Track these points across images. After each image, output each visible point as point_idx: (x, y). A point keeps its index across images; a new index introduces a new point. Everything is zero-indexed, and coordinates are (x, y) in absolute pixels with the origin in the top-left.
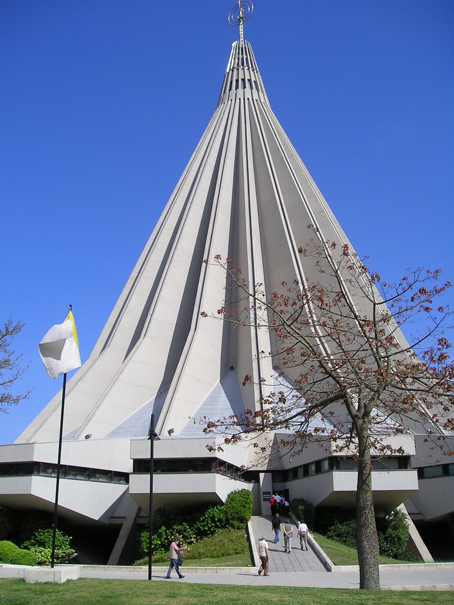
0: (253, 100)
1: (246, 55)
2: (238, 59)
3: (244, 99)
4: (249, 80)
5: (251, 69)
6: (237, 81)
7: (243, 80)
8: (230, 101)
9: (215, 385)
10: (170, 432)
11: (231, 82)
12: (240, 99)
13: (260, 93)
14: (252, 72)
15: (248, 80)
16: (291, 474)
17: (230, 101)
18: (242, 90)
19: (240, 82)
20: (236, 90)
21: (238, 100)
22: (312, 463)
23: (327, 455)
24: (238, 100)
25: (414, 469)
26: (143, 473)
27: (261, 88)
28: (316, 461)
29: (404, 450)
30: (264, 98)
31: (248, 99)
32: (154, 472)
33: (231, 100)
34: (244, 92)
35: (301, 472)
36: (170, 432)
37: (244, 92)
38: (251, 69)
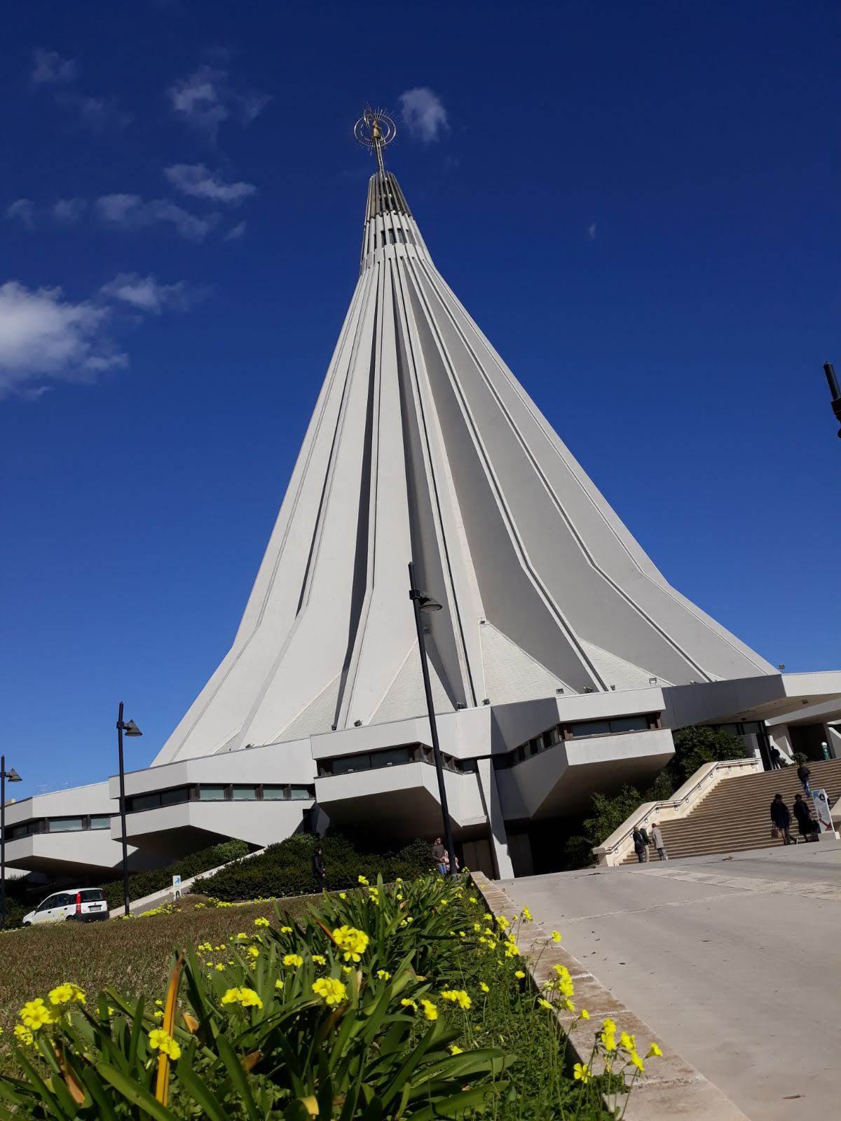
0: (408, 258)
1: (391, 192)
2: (381, 200)
3: (396, 259)
4: (400, 230)
6: (383, 233)
7: (391, 230)
11: (375, 236)
12: (390, 259)
13: (417, 246)
16: (517, 756)
19: (388, 234)
20: (383, 246)
22: (526, 744)
23: (554, 723)
26: (641, 730)
28: (544, 733)
30: (424, 254)
32: (126, 811)
33: (379, 263)
35: (528, 750)
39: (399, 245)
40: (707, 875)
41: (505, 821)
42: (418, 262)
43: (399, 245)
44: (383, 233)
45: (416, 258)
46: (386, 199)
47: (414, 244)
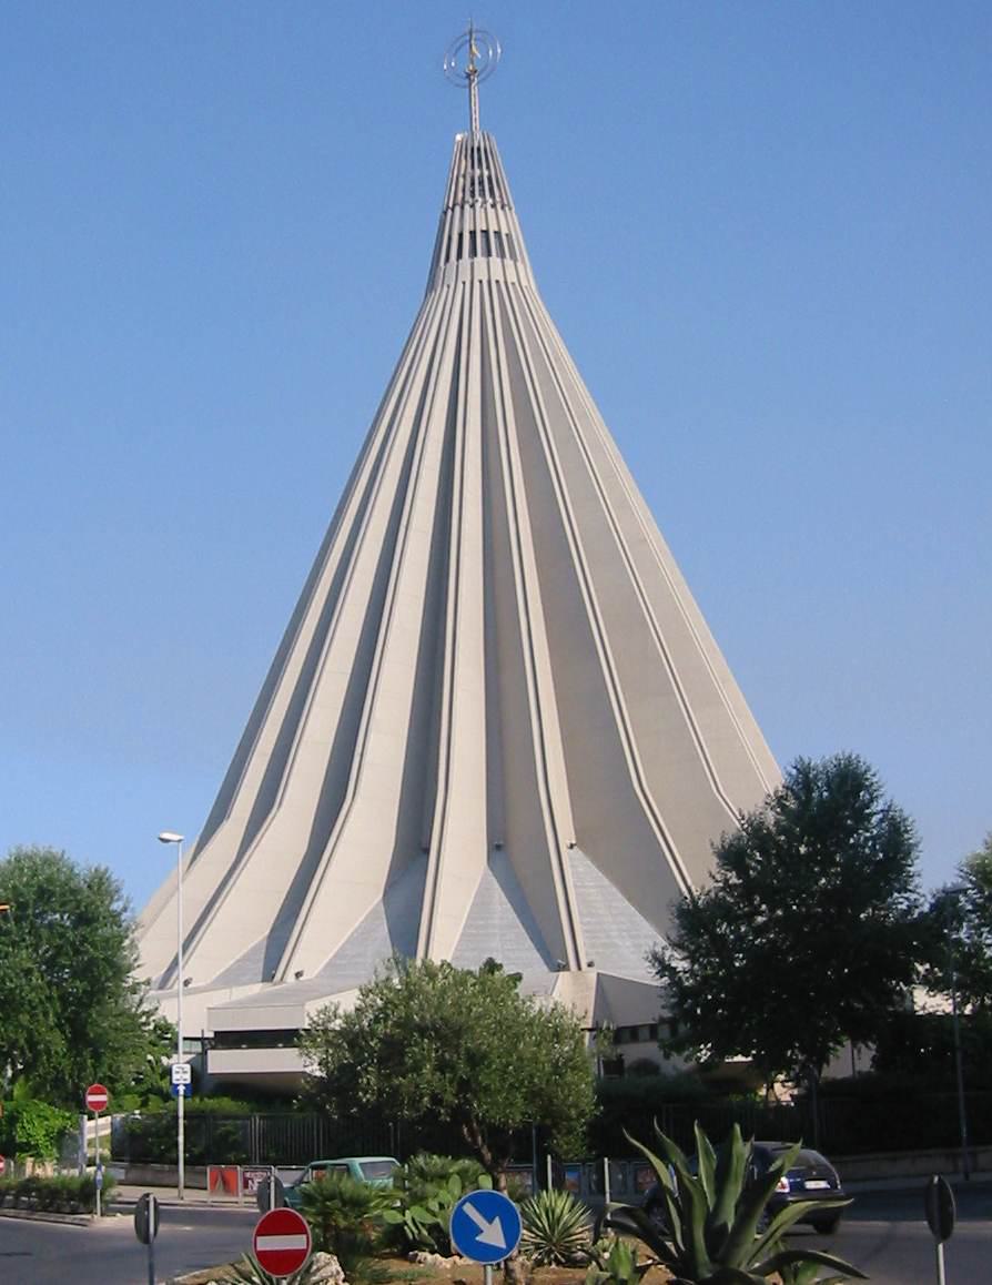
0: (506, 283)
1: (488, 167)
4: (498, 234)
5: (499, 206)
6: (473, 234)
8: (445, 288)
9: (376, 902)
10: (298, 975)
13: (519, 264)
14: (500, 211)
15: (495, 232)
17: (445, 288)
18: (499, 260)
21: (460, 286)
24: (460, 286)
25: (658, 1041)
27: (509, 248)
29: (657, 1018)
30: (528, 280)
31: (497, 282)
34: (472, 264)
36: (298, 975)
37: (472, 264)
38: (499, 206)
39: (495, 260)
40: (670, 1203)
41: (263, 981)
42: (519, 289)
43: (495, 260)
44: (473, 234)
45: (517, 284)
46: (481, 176)
47: (515, 261)
